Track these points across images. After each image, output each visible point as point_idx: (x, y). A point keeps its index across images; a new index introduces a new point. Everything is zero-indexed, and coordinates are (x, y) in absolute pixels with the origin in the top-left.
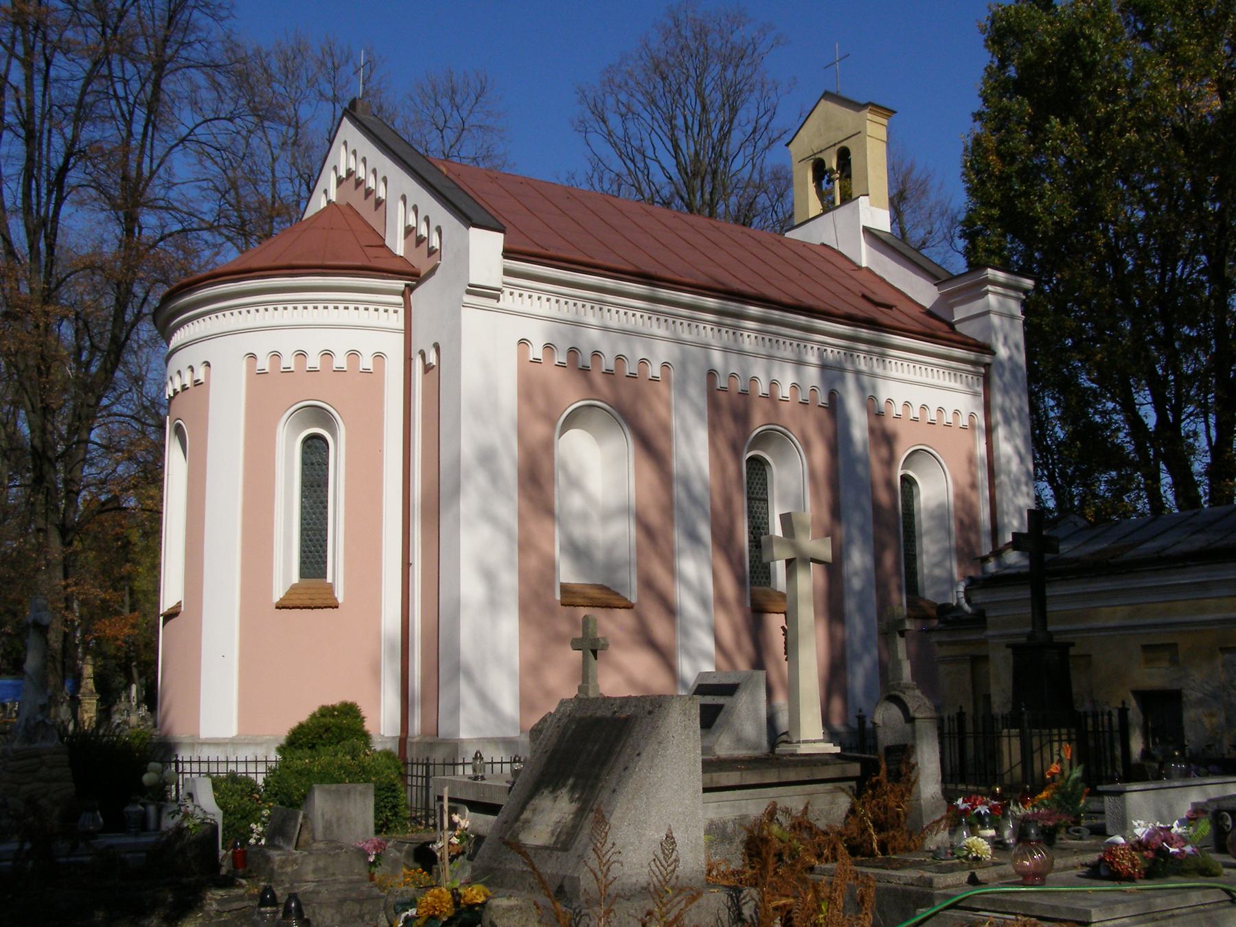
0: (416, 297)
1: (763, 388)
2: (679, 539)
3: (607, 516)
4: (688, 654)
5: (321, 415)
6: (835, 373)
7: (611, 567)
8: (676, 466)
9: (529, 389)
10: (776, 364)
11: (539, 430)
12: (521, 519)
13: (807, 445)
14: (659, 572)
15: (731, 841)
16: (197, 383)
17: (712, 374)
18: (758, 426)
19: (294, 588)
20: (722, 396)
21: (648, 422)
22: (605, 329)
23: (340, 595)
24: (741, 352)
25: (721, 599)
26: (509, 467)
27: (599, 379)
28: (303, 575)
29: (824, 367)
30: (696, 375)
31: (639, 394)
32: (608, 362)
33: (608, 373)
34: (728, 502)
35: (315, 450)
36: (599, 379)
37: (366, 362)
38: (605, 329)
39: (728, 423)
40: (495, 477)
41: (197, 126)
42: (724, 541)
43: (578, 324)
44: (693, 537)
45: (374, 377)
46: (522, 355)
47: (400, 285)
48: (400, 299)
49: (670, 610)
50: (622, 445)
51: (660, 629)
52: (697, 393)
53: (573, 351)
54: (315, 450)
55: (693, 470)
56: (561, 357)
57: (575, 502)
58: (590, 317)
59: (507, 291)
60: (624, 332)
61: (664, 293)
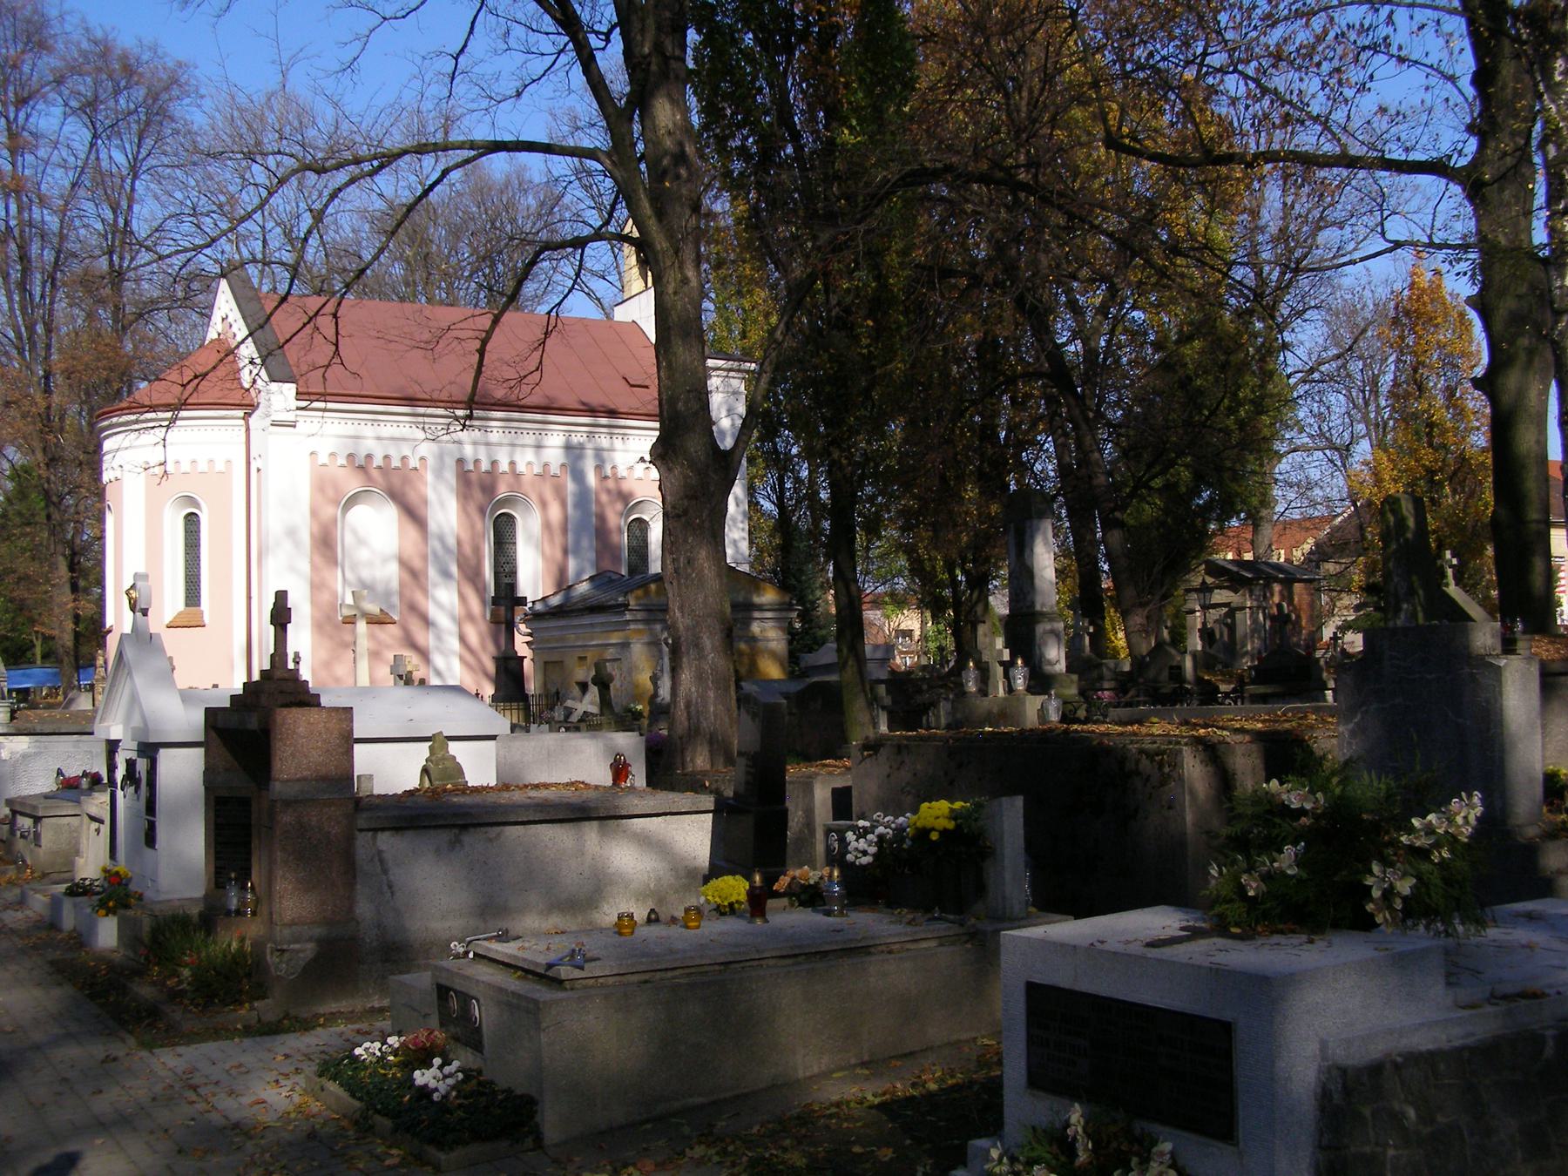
0: (253, 420)
1: (504, 466)
2: (432, 573)
3: (385, 560)
4: (442, 653)
5: (191, 500)
6: (578, 452)
7: (388, 594)
8: (432, 526)
9: (322, 485)
10: (518, 449)
11: (328, 511)
12: (314, 568)
13: (544, 505)
14: (419, 597)
15: (1229, 822)
16: (117, 479)
17: (461, 461)
18: (503, 491)
19: (180, 614)
20: (474, 477)
21: (412, 497)
22: (379, 438)
23: (206, 619)
24: (488, 444)
25: (470, 617)
26: (305, 537)
27: (375, 474)
28: (187, 605)
29: (568, 447)
30: (450, 463)
31: (406, 481)
32: (378, 461)
33: (379, 468)
34: (477, 551)
35: (192, 522)
36: (375, 474)
37: (220, 466)
38: (379, 438)
39: (478, 495)
40: (297, 544)
41: (166, 219)
42: (471, 574)
43: (357, 437)
44: (446, 574)
45: (225, 475)
46: (313, 462)
47: (241, 413)
48: (242, 422)
49: (427, 622)
50: (391, 512)
51: (421, 636)
52: (451, 476)
53: (351, 456)
54: (192, 522)
55: (447, 530)
56: (342, 461)
57: (363, 554)
58: (368, 431)
59: (301, 420)
60: (393, 439)
61: (421, 410)
